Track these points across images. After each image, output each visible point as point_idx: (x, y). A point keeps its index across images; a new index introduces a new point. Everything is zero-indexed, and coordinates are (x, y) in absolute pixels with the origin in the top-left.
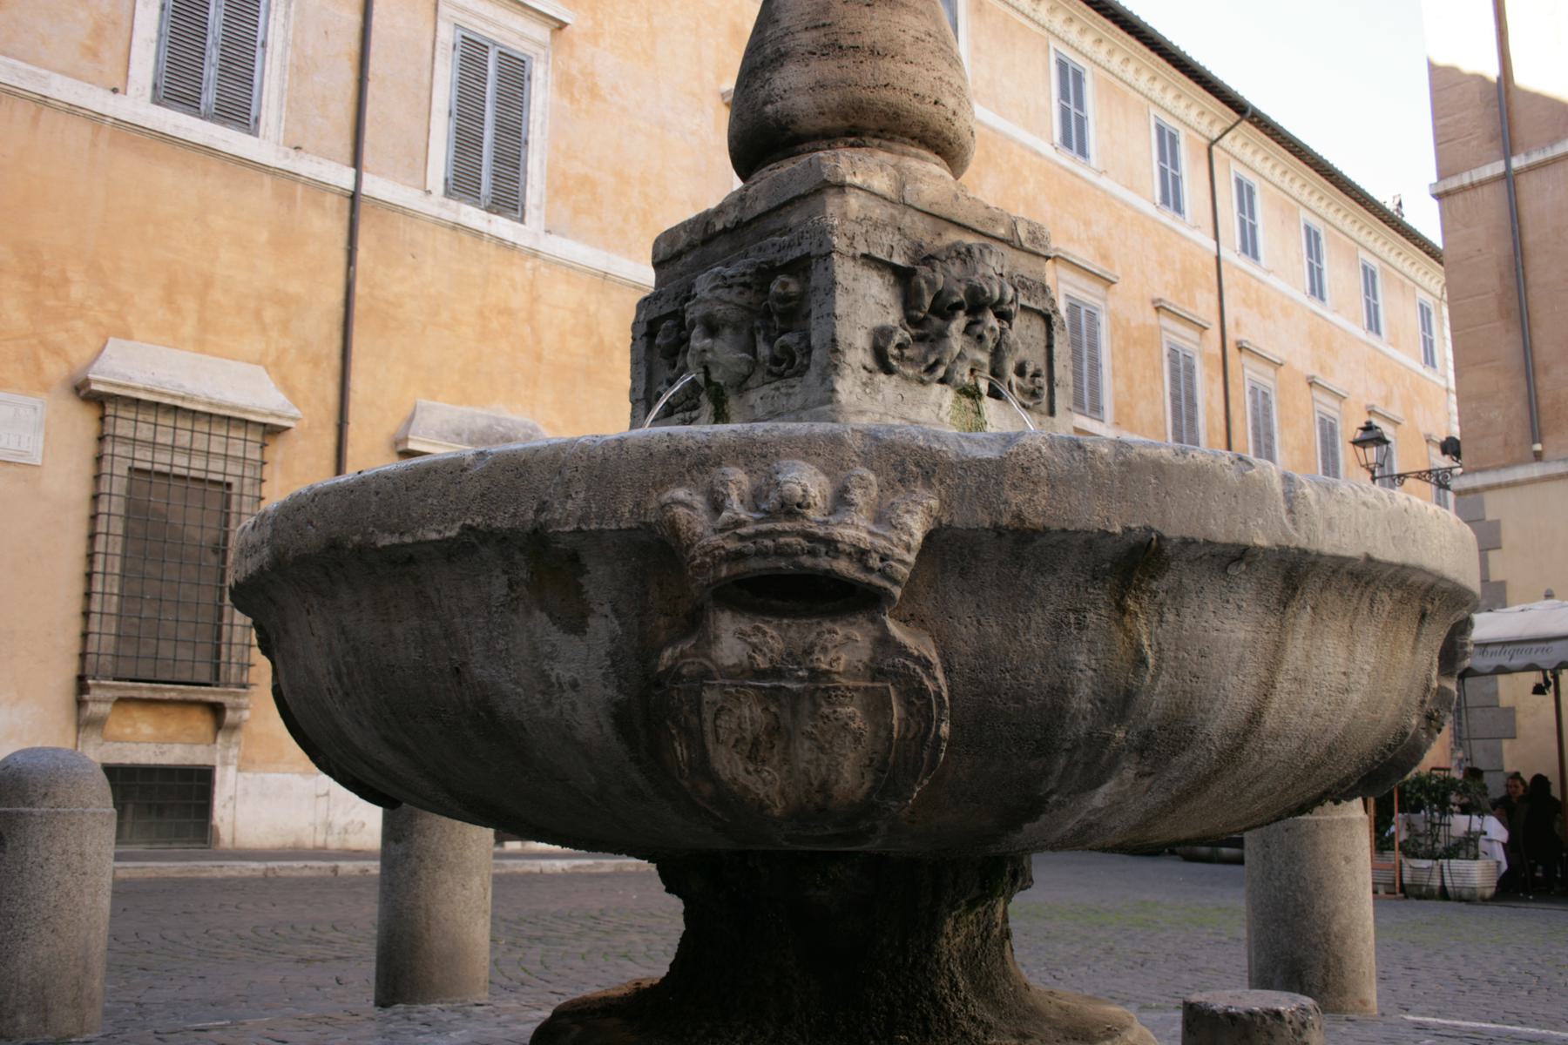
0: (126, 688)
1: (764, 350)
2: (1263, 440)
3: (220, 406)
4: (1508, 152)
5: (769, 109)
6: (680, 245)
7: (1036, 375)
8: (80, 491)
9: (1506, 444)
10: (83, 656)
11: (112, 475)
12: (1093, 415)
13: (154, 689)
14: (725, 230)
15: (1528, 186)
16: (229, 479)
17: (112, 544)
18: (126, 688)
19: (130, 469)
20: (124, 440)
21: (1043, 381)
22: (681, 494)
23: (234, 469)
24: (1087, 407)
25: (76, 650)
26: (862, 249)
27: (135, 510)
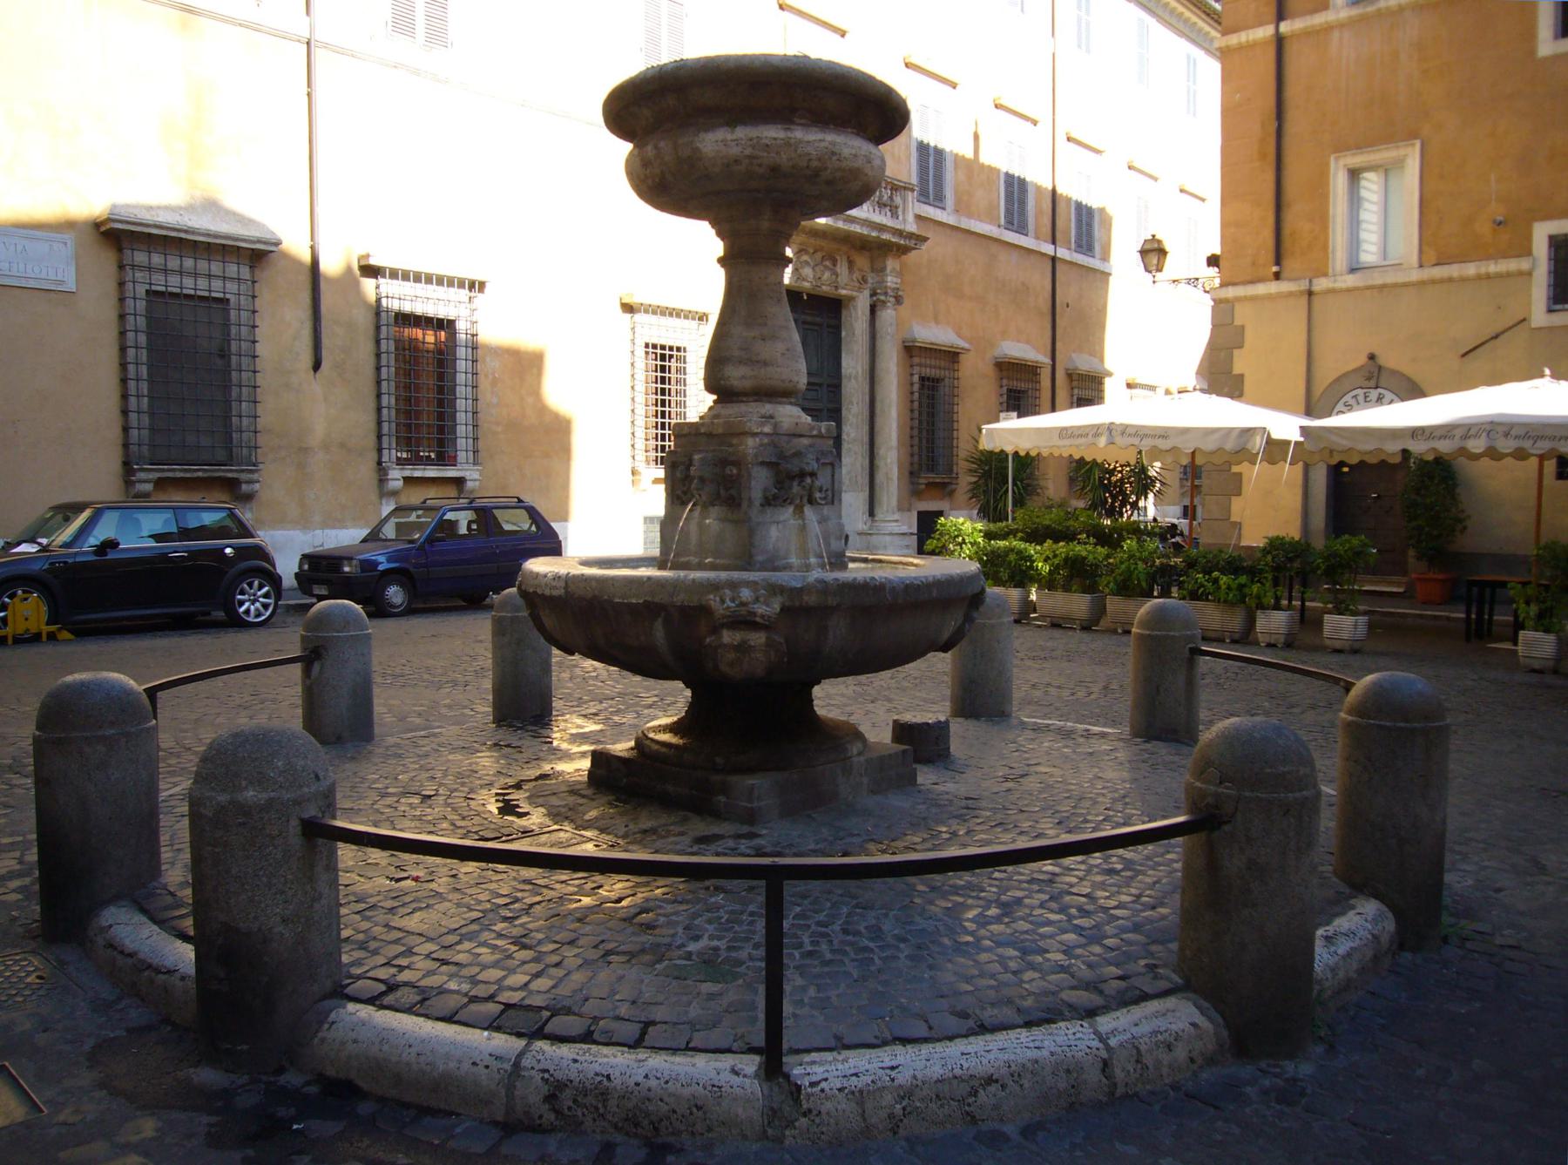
0: (163, 470)
1: (722, 492)
2: (1084, 218)
3: (216, 236)
4: (1281, 16)
5: (722, 382)
6: (685, 432)
7: (827, 490)
8: (109, 313)
9: (1254, 264)
10: (126, 446)
11: (135, 298)
12: (936, 204)
13: (186, 470)
14: (705, 434)
15: (1291, 51)
16: (228, 296)
17: (139, 355)
18: (163, 470)
19: (147, 291)
20: (141, 268)
21: (829, 493)
22: (712, 597)
23: (232, 287)
24: (931, 197)
25: (120, 441)
26: (761, 460)
27: (155, 326)
